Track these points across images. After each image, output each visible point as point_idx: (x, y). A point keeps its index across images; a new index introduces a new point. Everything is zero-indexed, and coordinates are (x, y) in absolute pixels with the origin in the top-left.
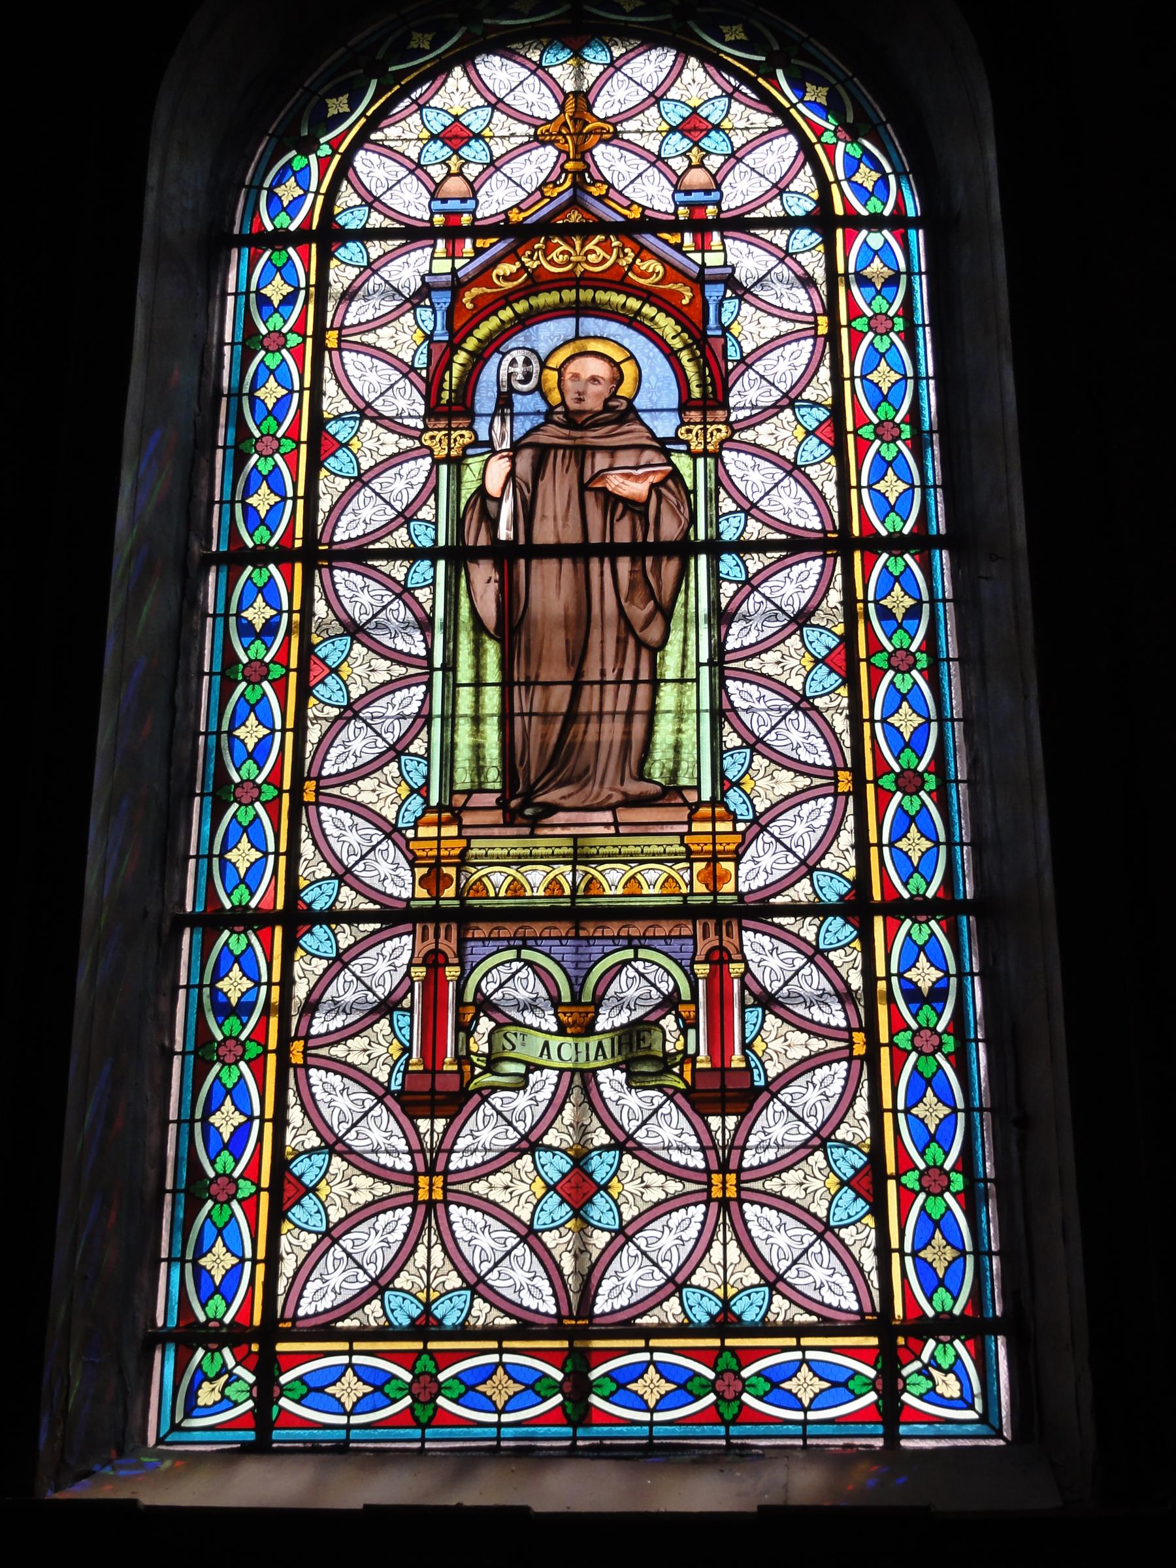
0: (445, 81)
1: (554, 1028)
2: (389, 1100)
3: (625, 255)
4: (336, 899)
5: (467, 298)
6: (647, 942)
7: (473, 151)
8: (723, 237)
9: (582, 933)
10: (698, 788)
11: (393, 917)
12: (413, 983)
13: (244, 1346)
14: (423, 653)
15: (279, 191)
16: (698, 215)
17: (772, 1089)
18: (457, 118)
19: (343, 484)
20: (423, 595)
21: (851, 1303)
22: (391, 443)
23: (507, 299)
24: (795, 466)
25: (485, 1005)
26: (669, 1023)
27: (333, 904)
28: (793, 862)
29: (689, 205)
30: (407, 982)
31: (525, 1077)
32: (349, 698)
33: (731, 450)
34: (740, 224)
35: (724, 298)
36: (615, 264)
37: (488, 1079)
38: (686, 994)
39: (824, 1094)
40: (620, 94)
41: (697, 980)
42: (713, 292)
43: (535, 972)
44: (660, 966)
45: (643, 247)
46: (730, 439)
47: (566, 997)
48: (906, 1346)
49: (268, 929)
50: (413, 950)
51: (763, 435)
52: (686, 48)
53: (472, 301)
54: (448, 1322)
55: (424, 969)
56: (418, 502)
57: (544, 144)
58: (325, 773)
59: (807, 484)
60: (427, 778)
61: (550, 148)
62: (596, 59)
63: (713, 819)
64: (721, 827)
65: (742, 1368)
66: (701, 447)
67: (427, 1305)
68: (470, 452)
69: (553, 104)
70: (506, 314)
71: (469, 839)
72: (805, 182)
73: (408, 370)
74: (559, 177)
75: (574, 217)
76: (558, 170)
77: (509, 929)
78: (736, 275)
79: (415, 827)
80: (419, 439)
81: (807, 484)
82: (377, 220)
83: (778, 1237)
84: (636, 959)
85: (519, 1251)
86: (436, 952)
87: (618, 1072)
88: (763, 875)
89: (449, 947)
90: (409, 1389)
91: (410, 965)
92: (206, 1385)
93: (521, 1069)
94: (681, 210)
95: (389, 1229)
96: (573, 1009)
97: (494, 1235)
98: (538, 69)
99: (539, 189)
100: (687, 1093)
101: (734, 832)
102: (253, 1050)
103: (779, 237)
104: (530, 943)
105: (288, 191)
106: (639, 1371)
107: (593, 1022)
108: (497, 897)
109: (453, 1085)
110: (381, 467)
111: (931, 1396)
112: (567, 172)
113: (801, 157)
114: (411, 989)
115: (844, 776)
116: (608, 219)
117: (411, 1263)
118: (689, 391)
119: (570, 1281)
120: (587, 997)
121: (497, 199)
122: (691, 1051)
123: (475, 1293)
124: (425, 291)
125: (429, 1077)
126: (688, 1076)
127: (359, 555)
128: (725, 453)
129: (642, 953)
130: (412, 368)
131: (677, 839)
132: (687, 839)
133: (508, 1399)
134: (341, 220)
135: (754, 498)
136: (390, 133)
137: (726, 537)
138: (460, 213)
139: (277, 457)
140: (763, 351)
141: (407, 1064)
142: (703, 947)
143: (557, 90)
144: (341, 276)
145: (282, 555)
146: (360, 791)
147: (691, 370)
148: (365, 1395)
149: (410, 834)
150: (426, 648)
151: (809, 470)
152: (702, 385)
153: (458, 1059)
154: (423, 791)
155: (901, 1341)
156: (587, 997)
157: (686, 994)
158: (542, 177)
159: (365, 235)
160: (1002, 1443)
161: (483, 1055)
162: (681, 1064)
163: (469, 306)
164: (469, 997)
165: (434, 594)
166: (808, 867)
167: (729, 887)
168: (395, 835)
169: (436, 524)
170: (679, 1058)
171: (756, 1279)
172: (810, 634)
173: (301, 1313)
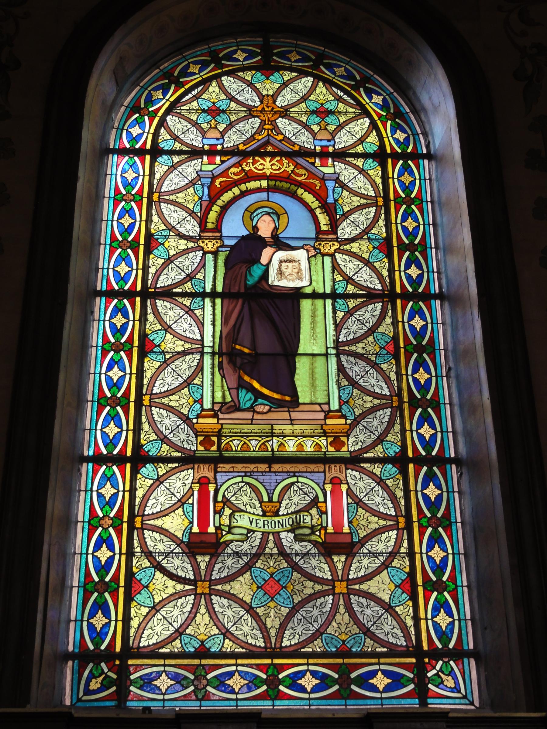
1: (261, 513)
8: (334, 161)
10: (328, 403)
12: (193, 491)
13: (112, 662)
14: (199, 338)
23: (236, 183)
25: (226, 502)
33: (339, 253)
35: (335, 187)
37: (229, 537)
38: (321, 499)
41: (326, 492)
42: (330, 184)
43: (250, 487)
45: (298, 163)
46: (339, 248)
47: (266, 499)
49: (123, 465)
53: (220, 184)
57: (254, 117)
68: (220, 249)
70: (236, 191)
71: (222, 424)
72: (373, 138)
74: (261, 131)
76: (261, 128)
79: (197, 418)
80: (197, 243)
82: (178, 146)
83: (368, 612)
84: (298, 482)
87: (290, 533)
89: (210, 475)
91: (192, 483)
92: (94, 681)
93: (245, 532)
95: (183, 606)
99: (252, 136)
101: (346, 424)
107: (278, 510)
108: (236, 451)
109: (214, 540)
112: (265, 129)
120: (275, 499)
121: (233, 140)
123: (225, 637)
126: (323, 536)
128: (336, 254)
129: (300, 479)
131: (319, 427)
132: (324, 427)
134: (161, 145)
140: (352, 211)
142: (329, 477)
146: (171, 401)
148: (171, 685)
149: (195, 421)
150: (201, 336)
153: (217, 528)
155: (426, 660)
156: (275, 499)
157: (321, 499)
160: (473, 707)
162: (320, 530)
164: (220, 498)
167: (344, 449)
173: (141, 645)
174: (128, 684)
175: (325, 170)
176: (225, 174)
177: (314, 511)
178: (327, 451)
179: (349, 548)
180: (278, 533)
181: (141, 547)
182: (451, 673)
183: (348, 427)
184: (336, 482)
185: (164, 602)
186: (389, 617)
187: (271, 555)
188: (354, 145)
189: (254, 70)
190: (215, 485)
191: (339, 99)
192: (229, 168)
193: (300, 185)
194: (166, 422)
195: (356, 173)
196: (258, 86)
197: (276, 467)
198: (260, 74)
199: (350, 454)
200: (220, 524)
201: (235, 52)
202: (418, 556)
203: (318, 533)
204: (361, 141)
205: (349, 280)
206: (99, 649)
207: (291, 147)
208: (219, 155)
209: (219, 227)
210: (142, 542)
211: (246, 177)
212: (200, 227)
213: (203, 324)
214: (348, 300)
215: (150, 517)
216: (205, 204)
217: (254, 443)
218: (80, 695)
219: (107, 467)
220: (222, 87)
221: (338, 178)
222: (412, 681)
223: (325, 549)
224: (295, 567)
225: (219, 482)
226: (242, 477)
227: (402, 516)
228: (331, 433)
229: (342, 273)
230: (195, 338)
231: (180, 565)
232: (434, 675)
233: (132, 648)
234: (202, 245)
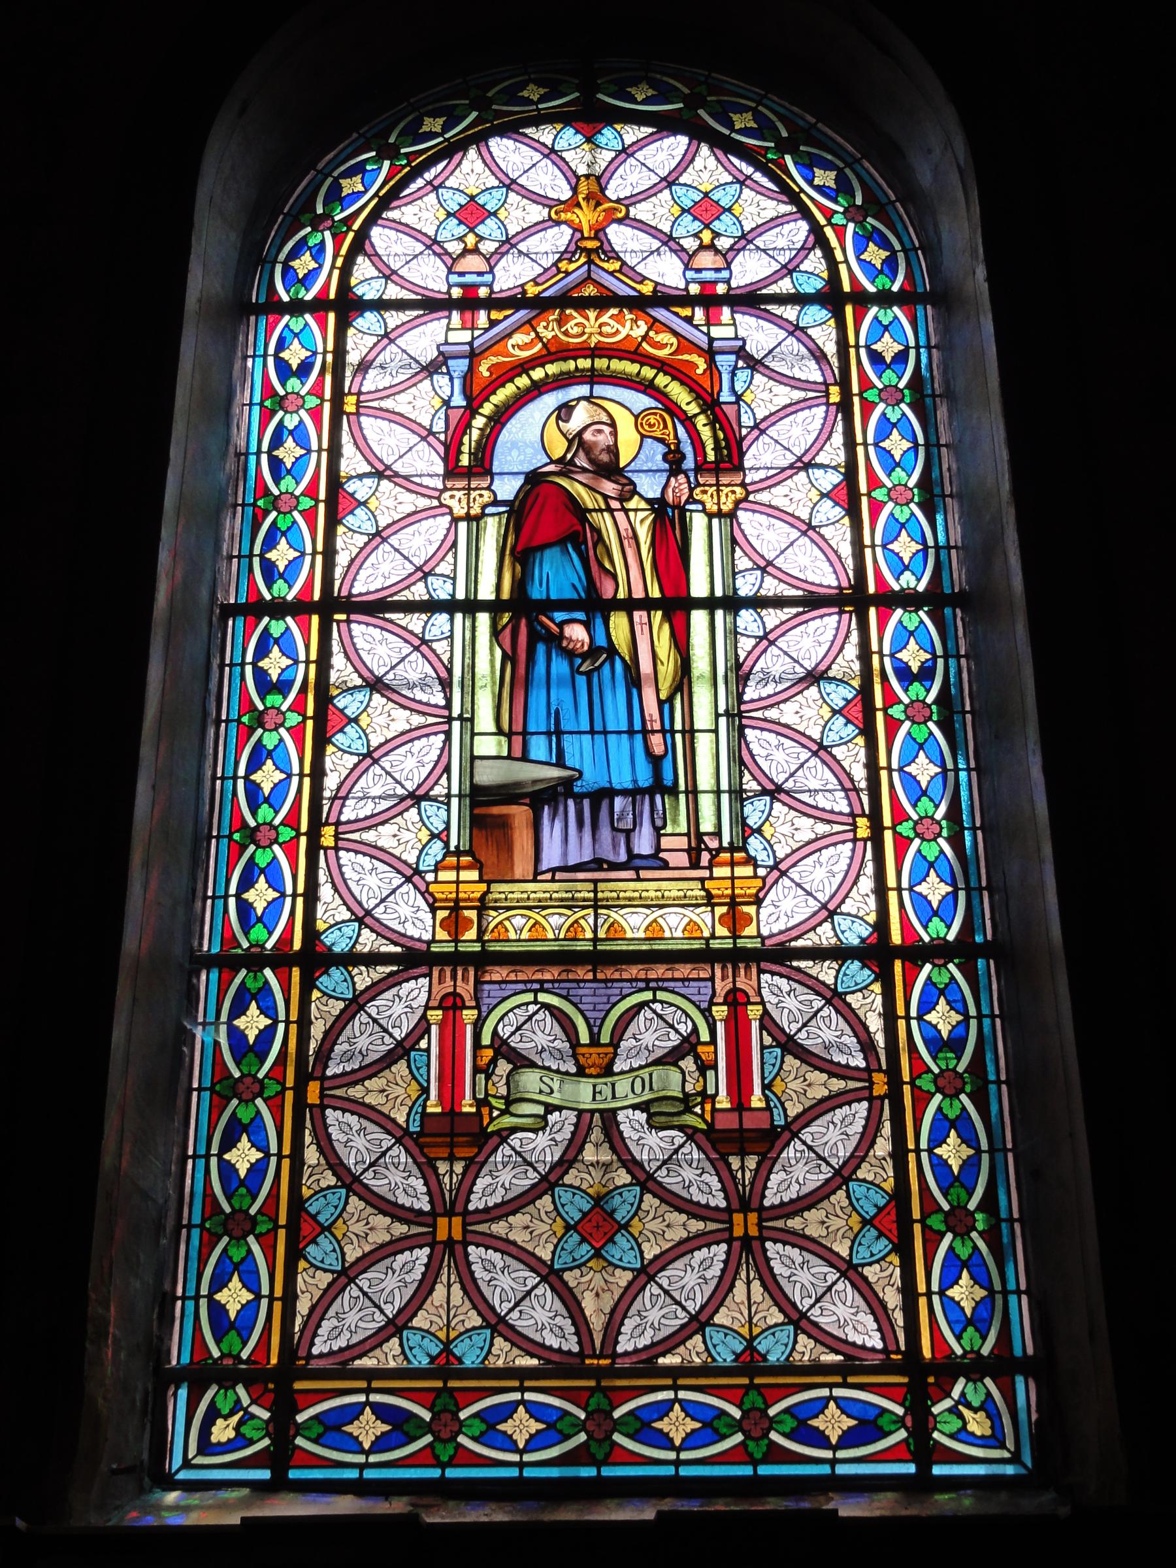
4: (356, 941)
6: (666, 984)
7: (488, 228)
8: (733, 312)
9: (600, 976)
11: (414, 959)
12: (429, 1025)
14: (442, 703)
15: (295, 264)
17: (793, 1129)
18: (472, 198)
19: (361, 540)
20: (441, 647)
21: (876, 1342)
22: (410, 502)
23: (524, 367)
25: (501, 1048)
27: (354, 946)
28: (814, 905)
31: (544, 1118)
32: (369, 746)
33: (746, 510)
35: (736, 368)
38: (705, 1036)
39: (552, 1139)
41: (715, 1021)
42: (725, 362)
43: (552, 1014)
44: (679, 1008)
45: (656, 320)
46: (745, 499)
47: (584, 1038)
48: (935, 1384)
50: (430, 992)
51: (776, 496)
52: (699, 134)
54: (772, 1358)
55: (725, 1008)
56: (437, 556)
60: (448, 824)
63: (732, 864)
64: (740, 871)
65: (768, 1406)
66: (715, 508)
67: (447, 1344)
68: (489, 510)
70: (523, 381)
72: (815, 262)
73: (428, 434)
75: (590, 291)
77: (528, 973)
78: (748, 348)
79: (436, 871)
82: (394, 292)
84: (654, 1001)
85: (840, 1286)
86: (734, 991)
88: (783, 919)
89: (466, 989)
90: (772, 1423)
91: (427, 1007)
92: (220, 1422)
93: (540, 1110)
96: (592, 1050)
99: (555, 264)
101: (755, 876)
102: (272, 1089)
103: (790, 312)
104: (546, 986)
105: (304, 264)
106: (664, 1409)
107: (612, 1062)
110: (399, 525)
111: (961, 1434)
114: (428, 1031)
115: (862, 822)
116: (621, 293)
117: (429, 1301)
118: (705, 455)
119: (593, 1319)
120: (605, 1038)
121: (511, 275)
122: (711, 1091)
125: (448, 1119)
126: (708, 1117)
127: (377, 608)
128: (740, 513)
129: (660, 995)
130: (431, 432)
132: (708, 884)
133: (522, 1441)
134: (359, 291)
136: (406, 213)
137: (742, 593)
138: (715, 283)
139: (295, 513)
141: (424, 1107)
142: (722, 987)
143: (569, 174)
144: (358, 345)
145: (300, 608)
147: (706, 433)
150: (445, 697)
152: (717, 448)
154: (441, 836)
156: (605, 1038)
157: (705, 1036)
159: (381, 305)
161: (501, 1097)
162: (702, 1104)
163: (486, 374)
164: (486, 1040)
165: (452, 646)
167: (750, 930)
168: (416, 879)
169: (454, 579)
171: (780, 1318)
177: (688, 1064)
178: (713, 936)
180: (614, 1111)
183: (759, 883)
185: (665, 1260)
186: (549, 1293)
189: (557, 122)
191: (743, 182)
193: (662, 366)
194: (368, 879)
198: (572, 131)
199: (763, 943)
203: (698, 1110)
204: (788, 270)
207: (638, 287)
208: (485, 308)
210: (321, 1134)
211: (544, 352)
214: (426, 597)
216: (456, 416)
217: (518, 921)
220: (491, 164)
221: (743, 348)
222: (900, 1422)
234: (448, 502)
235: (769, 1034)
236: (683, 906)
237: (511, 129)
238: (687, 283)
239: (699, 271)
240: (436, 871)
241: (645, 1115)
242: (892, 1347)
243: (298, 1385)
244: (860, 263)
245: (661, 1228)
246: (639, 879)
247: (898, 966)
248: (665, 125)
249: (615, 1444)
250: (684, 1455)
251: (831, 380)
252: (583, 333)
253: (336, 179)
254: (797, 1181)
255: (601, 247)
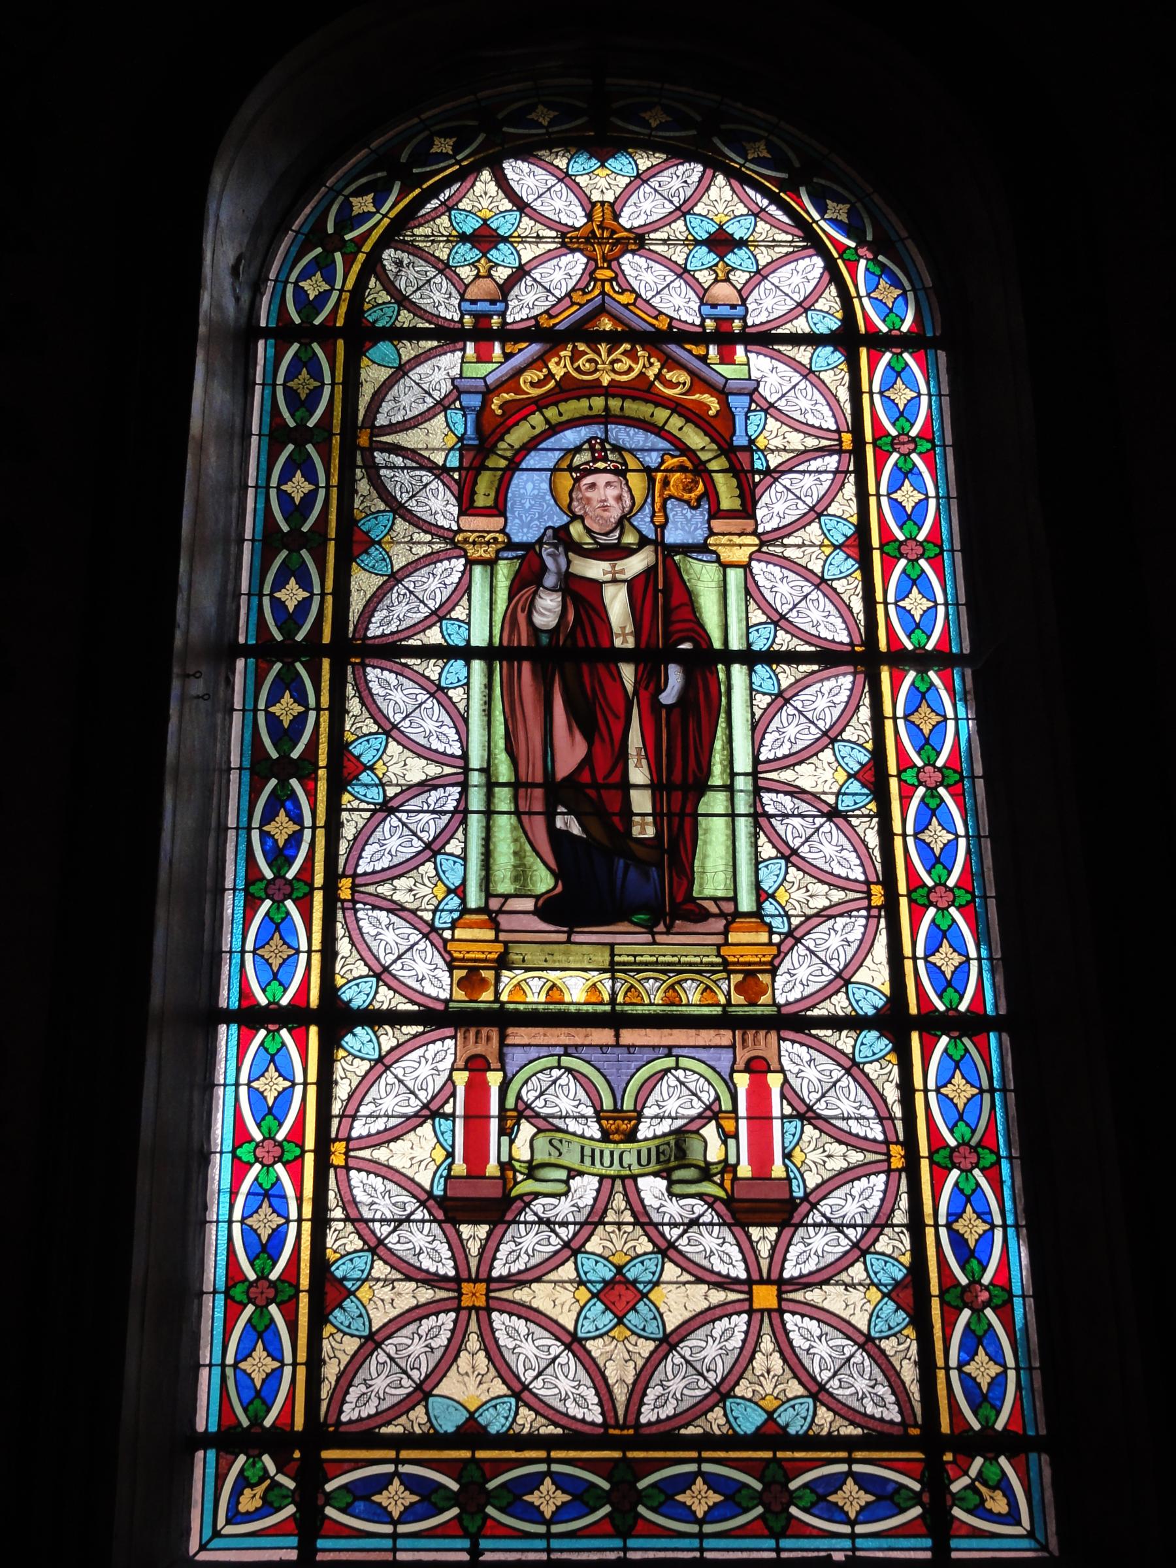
0: (473, 185)
1: (598, 1135)
2: (431, 1203)
3: (651, 364)
5: (496, 403)
8: (747, 351)
10: (734, 899)
12: (455, 1087)
14: (459, 752)
16: (724, 328)
20: (457, 695)
24: (823, 580)
25: (524, 1112)
26: (710, 1131)
29: (716, 319)
30: (449, 1087)
31: (566, 1182)
33: (759, 561)
34: (765, 339)
35: (749, 410)
36: (642, 374)
38: (726, 1105)
40: (647, 206)
42: (738, 403)
47: (608, 1104)
48: (954, 1462)
52: (715, 164)
53: (500, 407)
54: (493, 1430)
57: (573, 251)
58: (360, 870)
59: (834, 596)
61: (578, 255)
62: (622, 167)
69: (580, 213)
71: (506, 944)
72: (830, 301)
79: (453, 928)
81: (834, 596)
84: (677, 1068)
91: (452, 1069)
93: (563, 1174)
94: (708, 322)
97: (537, 1343)
98: (565, 177)
99: (568, 295)
100: (729, 1202)
101: (770, 943)
106: (836, 1483)
107: (635, 1129)
109: (495, 1192)
113: (827, 277)
120: (628, 1104)
121: (525, 305)
124: (458, 390)
126: (727, 1184)
128: (754, 563)
129: (684, 1062)
132: (724, 951)
135: (784, 609)
138: (732, 320)
140: (828, 1186)
141: (449, 1168)
142: (743, 1056)
151: (835, 584)
153: (503, 1166)
156: (628, 1104)
157: (726, 1105)
158: (572, 283)
162: (722, 1172)
163: (499, 412)
166: (843, 980)
170: (720, 1167)
172: (843, 749)
174: (320, 1502)
175: (726, 370)
176: (511, 384)
179: (784, 1210)
181: (344, 1209)
182: (1003, 1485)
184: (758, 1068)
187: (619, 1224)
188: (789, 316)
190: (501, 1074)
191: (758, 214)
192: (520, 371)
195: (797, 377)
196: (583, 181)
197: (629, 1036)
200: (511, 1158)
201: (532, 108)
202: (930, 1232)
205: (779, 620)
206: (261, 1425)
209: (500, 505)
212: (460, 506)
213: (466, 721)
215: (363, 1143)
218: (220, 1525)
219: (269, 1031)
223: (733, 1214)
224: (666, 1250)
225: (511, 1069)
226: (560, 1056)
227: (897, 1143)
228: (738, 963)
229: (765, 606)
230: (449, 752)
231: (427, 1246)
232: (966, 1488)
233: (326, 1424)
235: (789, 1104)
236: (699, 972)
237: (526, 152)
238: (703, 321)
239: (714, 306)
240: (453, 928)
241: (665, 1183)
242: (910, 1421)
243: (326, 1454)
244: (883, 304)
245: (556, 1299)
246: (654, 943)
247: (915, 1037)
248: (679, 153)
249: (791, 1517)
250: (402, 1529)
251: (843, 428)
252: (596, 370)
253: (347, 198)
254: (526, 1253)
255: (615, 279)
